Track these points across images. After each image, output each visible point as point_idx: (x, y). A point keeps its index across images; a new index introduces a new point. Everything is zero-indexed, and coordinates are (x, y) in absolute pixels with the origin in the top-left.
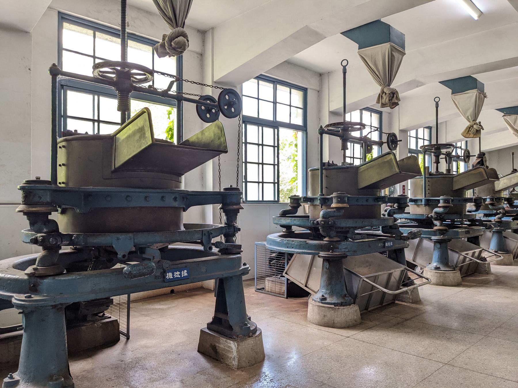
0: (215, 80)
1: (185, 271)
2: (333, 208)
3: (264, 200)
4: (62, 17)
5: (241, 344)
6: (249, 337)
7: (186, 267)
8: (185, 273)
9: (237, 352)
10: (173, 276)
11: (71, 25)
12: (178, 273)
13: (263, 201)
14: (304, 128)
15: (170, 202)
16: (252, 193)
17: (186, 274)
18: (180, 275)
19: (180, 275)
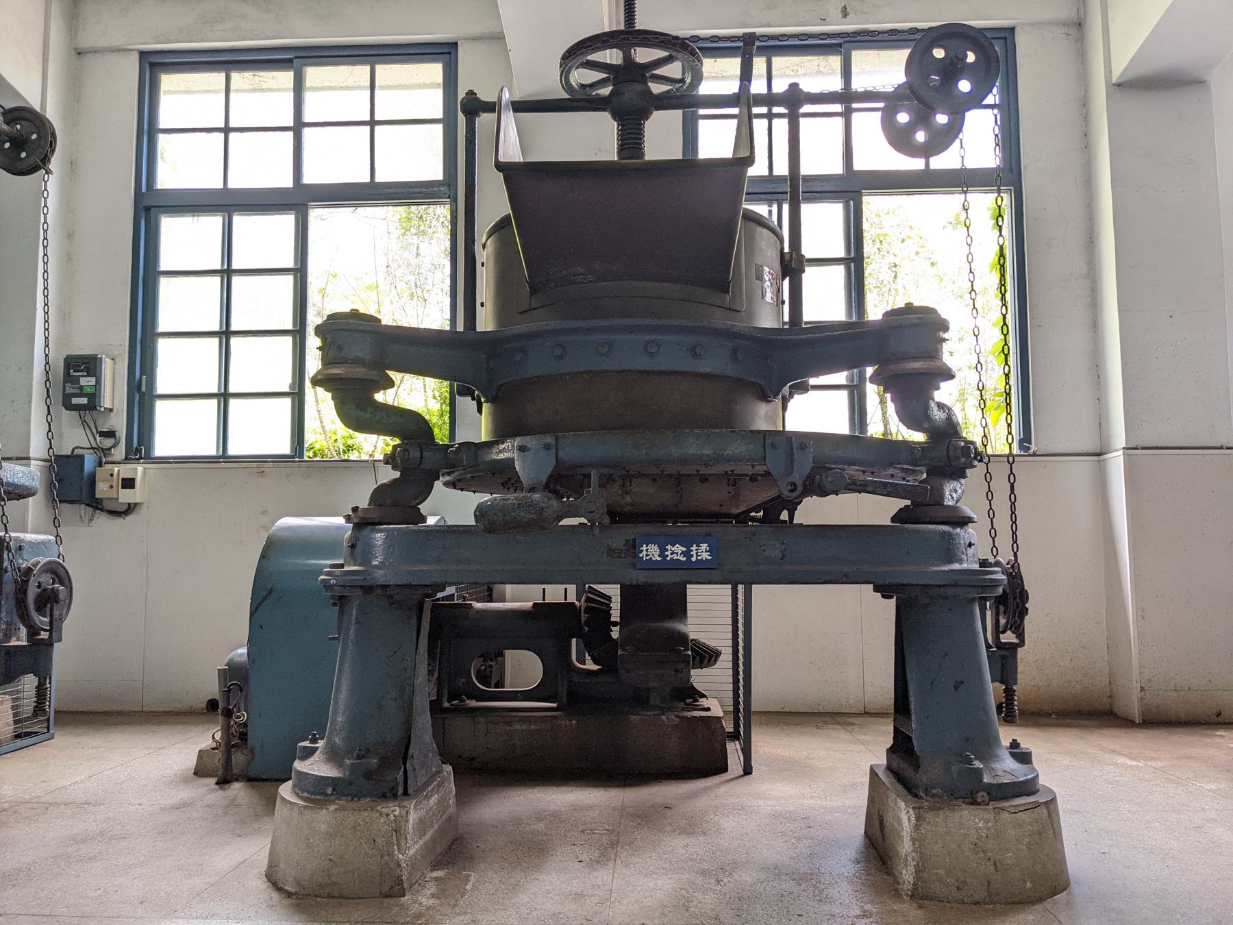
0: (1114, 81)
1: (704, 546)
2: (381, 531)
3: (232, 451)
4: (152, 65)
5: (930, 816)
6: (974, 803)
7: (708, 535)
8: (702, 552)
9: (913, 840)
10: (662, 554)
11: (719, 60)
12: (679, 549)
13: (223, 458)
14: (150, 206)
15: (716, 362)
16: (180, 431)
17: (706, 556)
18: (687, 554)
19: (687, 554)
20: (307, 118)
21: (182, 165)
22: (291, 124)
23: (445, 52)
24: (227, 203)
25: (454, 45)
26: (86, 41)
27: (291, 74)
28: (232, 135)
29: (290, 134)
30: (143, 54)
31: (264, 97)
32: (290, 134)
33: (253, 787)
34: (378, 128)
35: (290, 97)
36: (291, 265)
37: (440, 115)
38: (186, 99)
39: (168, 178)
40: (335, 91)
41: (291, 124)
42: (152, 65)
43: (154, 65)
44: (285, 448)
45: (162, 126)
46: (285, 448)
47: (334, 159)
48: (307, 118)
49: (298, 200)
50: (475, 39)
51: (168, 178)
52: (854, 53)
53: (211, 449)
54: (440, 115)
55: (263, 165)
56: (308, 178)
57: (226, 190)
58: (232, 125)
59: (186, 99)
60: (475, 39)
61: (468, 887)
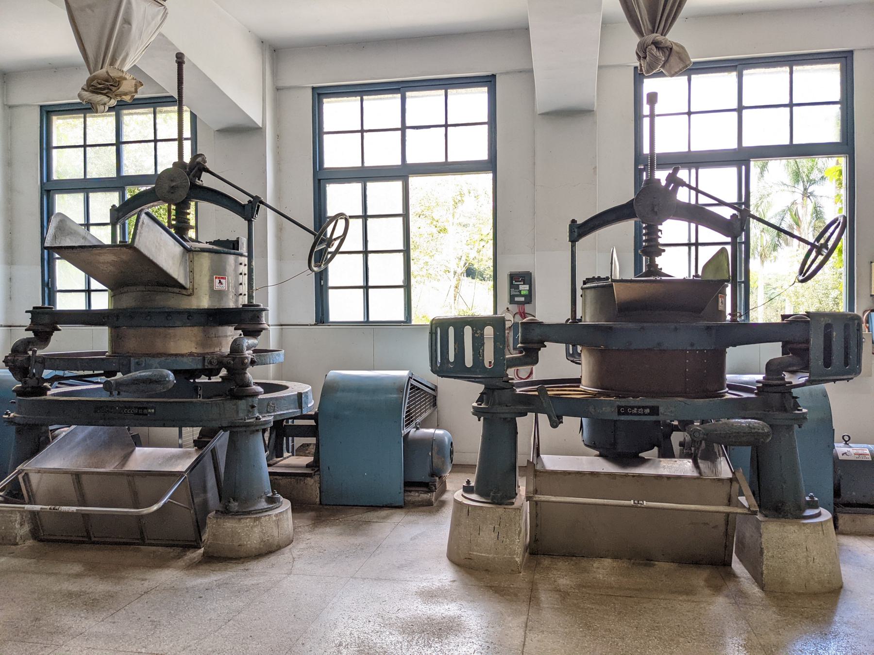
3: (371, 319)
4: (319, 94)
14: (323, 177)
20: (745, 104)
21: (339, 153)
22: (114, 142)
23: (489, 81)
24: (364, 175)
25: (494, 76)
26: (281, 84)
27: (399, 95)
28: (159, 144)
29: (399, 132)
30: (313, 88)
31: (383, 109)
32: (399, 132)
33: (471, 574)
34: (449, 128)
35: (788, 75)
36: (401, 212)
37: (486, 120)
38: (338, 112)
39: (331, 161)
40: (425, 105)
41: (114, 142)
42: (319, 94)
43: (319, 94)
44: (401, 317)
45: (325, 130)
46: (401, 317)
47: (424, 148)
48: (745, 104)
49: (402, 173)
50: (507, 73)
51: (331, 161)
52: (745, 72)
53: (360, 318)
54: (486, 120)
55: (383, 152)
56: (410, 160)
57: (363, 168)
58: (158, 138)
59: (338, 112)
60: (507, 73)
61: (271, 418)
